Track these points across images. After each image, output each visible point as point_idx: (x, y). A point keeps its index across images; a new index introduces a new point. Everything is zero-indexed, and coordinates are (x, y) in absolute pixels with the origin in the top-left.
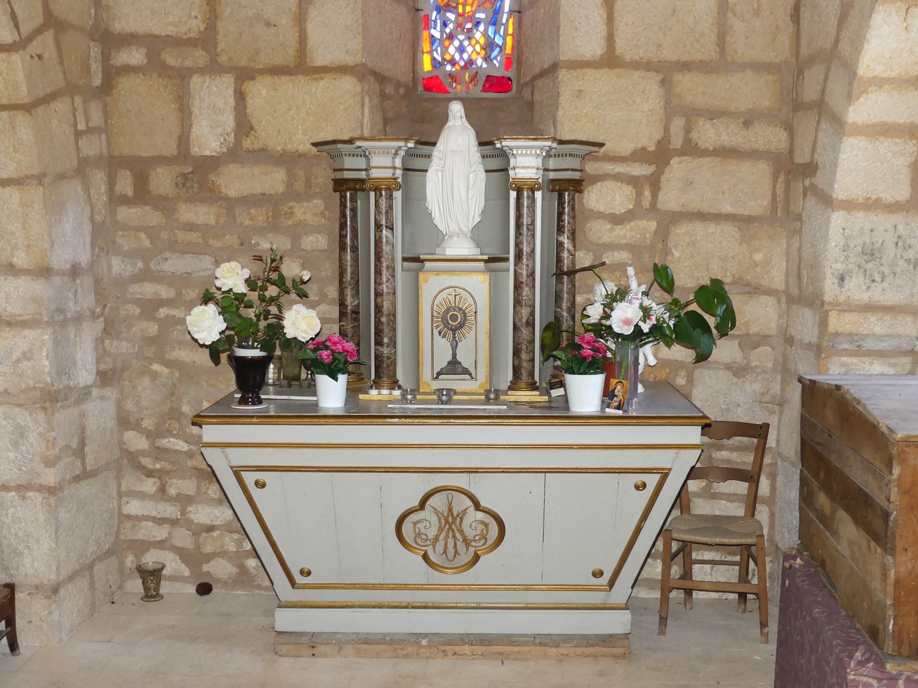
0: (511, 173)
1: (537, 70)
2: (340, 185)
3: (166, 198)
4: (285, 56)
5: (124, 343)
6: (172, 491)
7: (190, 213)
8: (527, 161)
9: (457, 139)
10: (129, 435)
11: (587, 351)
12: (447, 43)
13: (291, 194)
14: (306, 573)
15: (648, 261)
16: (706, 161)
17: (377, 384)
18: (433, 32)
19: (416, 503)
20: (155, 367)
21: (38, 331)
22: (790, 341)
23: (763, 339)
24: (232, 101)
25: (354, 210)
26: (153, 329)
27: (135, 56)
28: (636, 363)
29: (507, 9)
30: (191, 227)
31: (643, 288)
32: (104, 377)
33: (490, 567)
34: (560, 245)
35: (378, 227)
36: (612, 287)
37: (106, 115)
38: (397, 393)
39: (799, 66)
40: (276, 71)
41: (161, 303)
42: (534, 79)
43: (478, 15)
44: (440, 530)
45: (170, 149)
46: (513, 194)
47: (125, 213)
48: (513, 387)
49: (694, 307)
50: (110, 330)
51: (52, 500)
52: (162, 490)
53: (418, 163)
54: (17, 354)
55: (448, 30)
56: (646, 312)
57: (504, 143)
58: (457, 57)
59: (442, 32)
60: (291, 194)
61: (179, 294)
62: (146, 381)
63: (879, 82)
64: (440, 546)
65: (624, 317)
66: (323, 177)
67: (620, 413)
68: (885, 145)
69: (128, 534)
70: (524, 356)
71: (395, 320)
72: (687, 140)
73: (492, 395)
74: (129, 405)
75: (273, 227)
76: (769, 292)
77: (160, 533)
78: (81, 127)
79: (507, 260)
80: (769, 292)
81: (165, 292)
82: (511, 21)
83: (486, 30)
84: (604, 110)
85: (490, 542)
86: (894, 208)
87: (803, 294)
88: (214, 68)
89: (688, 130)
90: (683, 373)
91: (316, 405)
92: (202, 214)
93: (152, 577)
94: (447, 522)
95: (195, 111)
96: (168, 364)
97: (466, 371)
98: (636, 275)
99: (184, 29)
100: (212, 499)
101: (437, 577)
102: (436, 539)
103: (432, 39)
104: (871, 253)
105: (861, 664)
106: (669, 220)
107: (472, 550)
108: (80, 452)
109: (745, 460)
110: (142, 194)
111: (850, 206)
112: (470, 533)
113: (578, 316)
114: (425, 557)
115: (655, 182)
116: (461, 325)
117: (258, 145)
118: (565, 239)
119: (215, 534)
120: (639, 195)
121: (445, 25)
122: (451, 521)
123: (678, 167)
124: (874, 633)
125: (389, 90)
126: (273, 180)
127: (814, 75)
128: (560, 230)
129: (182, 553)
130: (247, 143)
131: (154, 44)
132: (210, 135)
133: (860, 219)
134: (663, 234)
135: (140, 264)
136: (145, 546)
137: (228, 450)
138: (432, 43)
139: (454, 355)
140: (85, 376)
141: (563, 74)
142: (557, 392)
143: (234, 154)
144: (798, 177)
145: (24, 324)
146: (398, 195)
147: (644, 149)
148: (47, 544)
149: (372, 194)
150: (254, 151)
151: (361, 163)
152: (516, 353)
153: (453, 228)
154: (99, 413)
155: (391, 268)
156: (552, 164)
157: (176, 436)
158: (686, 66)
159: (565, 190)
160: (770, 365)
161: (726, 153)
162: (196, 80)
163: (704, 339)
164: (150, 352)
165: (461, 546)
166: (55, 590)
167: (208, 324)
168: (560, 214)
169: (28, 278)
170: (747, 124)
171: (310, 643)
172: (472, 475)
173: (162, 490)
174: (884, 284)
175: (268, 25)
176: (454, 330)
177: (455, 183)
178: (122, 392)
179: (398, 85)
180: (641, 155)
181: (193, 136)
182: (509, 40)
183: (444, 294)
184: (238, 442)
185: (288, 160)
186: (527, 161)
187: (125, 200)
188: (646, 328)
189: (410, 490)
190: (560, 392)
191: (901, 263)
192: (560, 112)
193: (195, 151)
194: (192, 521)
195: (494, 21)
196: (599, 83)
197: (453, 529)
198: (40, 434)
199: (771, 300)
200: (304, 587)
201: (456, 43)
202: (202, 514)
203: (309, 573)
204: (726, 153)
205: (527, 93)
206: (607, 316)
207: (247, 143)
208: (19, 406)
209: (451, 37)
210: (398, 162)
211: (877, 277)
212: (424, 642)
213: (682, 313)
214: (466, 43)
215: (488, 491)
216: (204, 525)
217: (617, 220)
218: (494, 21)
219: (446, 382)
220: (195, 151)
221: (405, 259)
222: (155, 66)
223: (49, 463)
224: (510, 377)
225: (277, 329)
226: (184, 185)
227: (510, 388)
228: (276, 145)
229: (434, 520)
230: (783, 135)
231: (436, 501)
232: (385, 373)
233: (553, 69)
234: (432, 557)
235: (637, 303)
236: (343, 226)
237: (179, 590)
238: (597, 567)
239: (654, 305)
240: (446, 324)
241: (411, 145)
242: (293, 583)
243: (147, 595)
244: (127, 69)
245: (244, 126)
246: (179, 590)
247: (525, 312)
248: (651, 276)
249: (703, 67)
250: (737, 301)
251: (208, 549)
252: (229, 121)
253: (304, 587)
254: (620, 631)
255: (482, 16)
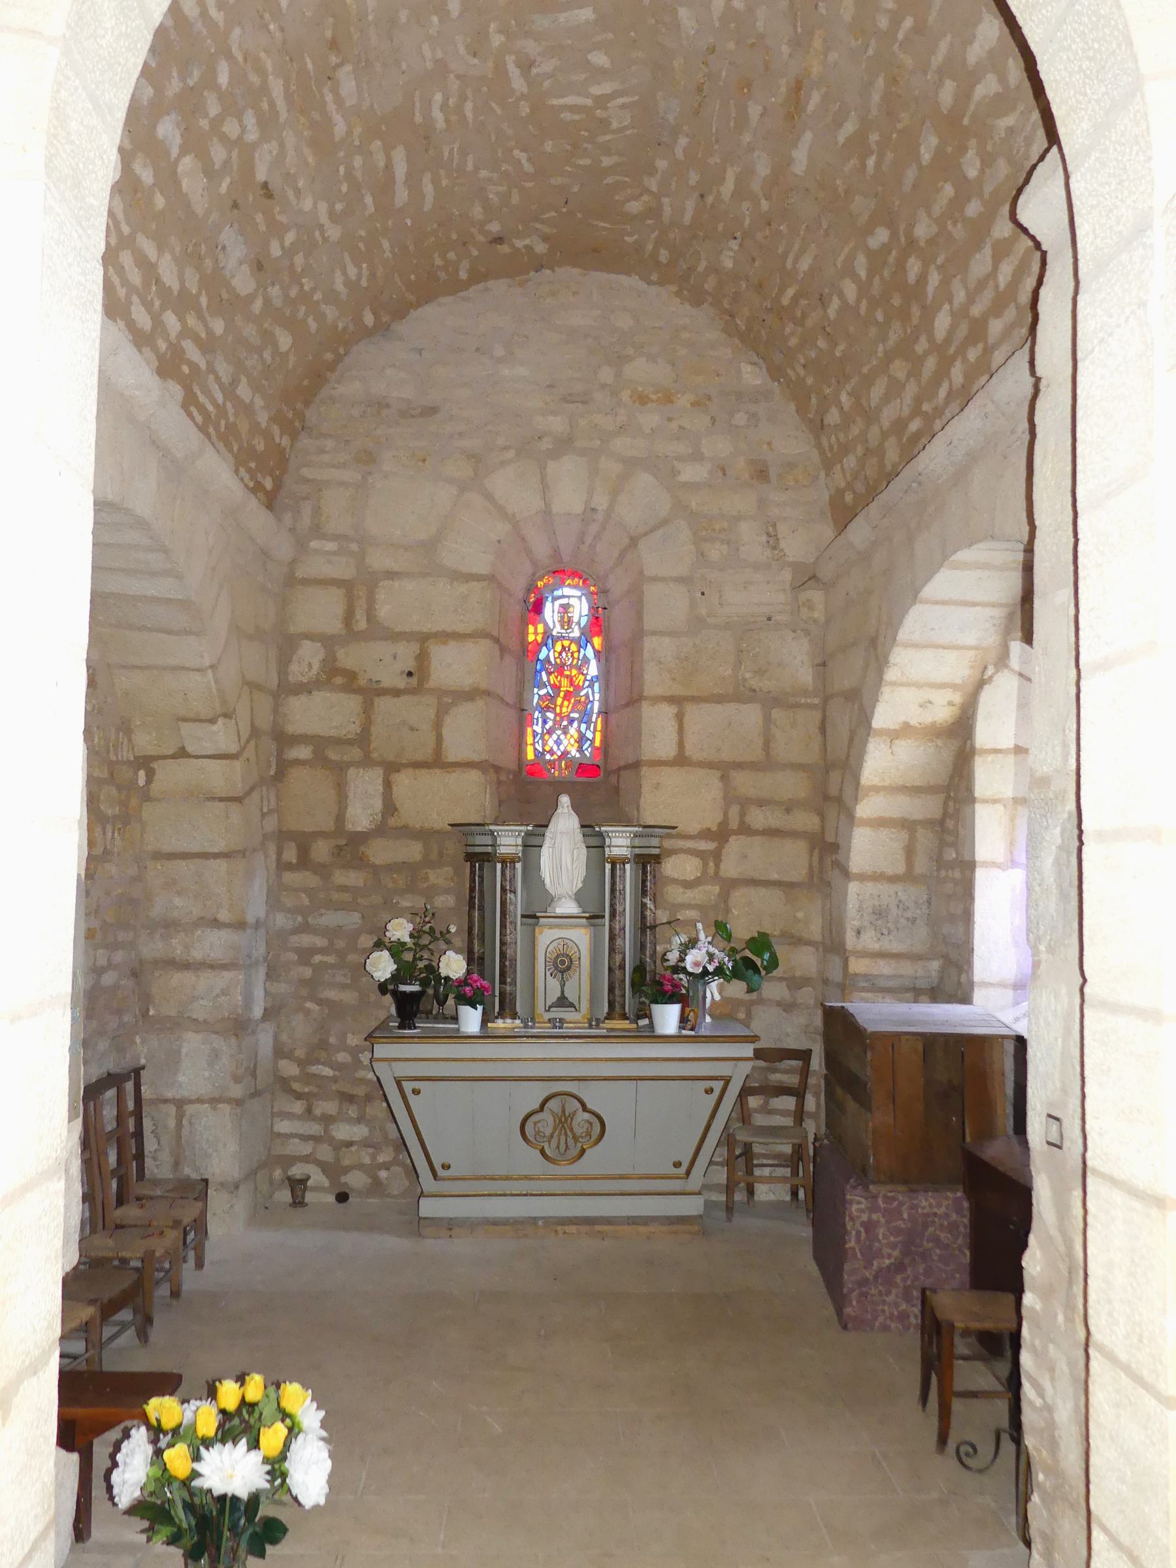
0: (607, 850)
1: (622, 763)
2: (471, 857)
3: (323, 866)
4: (425, 752)
5: (283, 985)
6: (318, 1112)
7: (341, 877)
8: (620, 842)
9: (565, 823)
10: (283, 1063)
11: (668, 987)
12: (546, 737)
13: (427, 862)
14: (446, 1167)
15: (712, 917)
16: (757, 840)
17: (501, 1015)
18: (535, 727)
19: (537, 1106)
20: (308, 1005)
21: (234, 972)
22: (826, 982)
23: (805, 981)
24: (381, 788)
25: (481, 877)
26: (307, 972)
27: (303, 752)
28: (704, 997)
29: (596, 710)
30: (343, 889)
31: (710, 939)
32: (268, 1014)
33: (595, 1160)
34: (644, 905)
35: (503, 890)
36: (684, 938)
37: (278, 798)
38: (518, 1022)
39: (828, 766)
40: (417, 765)
41: (314, 951)
42: (620, 769)
43: (572, 715)
44: (555, 1129)
45: (328, 824)
46: (608, 866)
47: (289, 877)
48: (609, 1017)
49: (748, 953)
50: (272, 974)
51: (238, 1111)
52: (309, 1110)
53: (535, 841)
54: (218, 991)
55: (547, 727)
56: (711, 957)
57: (603, 829)
58: (555, 748)
59: (543, 727)
60: (427, 862)
61: (331, 943)
62: (300, 1017)
63: (876, 789)
64: (554, 1142)
65: (694, 959)
66: (454, 849)
67: (693, 1033)
68: (884, 834)
69: (278, 1150)
70: (617, 992)
71: (1027, 846)
72: (742, 822)
73: (594, 1022)
74: (284, 1037)
75: (411, 889)
76: (809, 943)
77: (306, 1149)
78: (265, 810)
79: (603, 917)
80: (809, 943)
81: (320, 942)
82: (599, 720)
83: (579, 727)
84: (677, 800)
85: (594, 1137)
86: (893, 879)
87: (833, 945)
88: (367, 762)
89: (743, 814)
90: (743, 1009)
91: (458, 1030)
92: (353, 878)
93: (298, 1186)
94: (560, 1121)
95: (351, 795)
96: (320, 1002)
97: (572, 1005)
98: (704, 929)
99: (344, 732)
100: (351, 1118)
101: (552, 1169)
102: (552, 1136)
103: (535, 734)
104: (879, 913)
105: (855, 1187)
106: (729, 885)
107: (579, 1145)
108: (254, 1075)
109: (793, 1080)
110: (304, 862)
111: (862, 878)
112: (578, 1131)
113: (658, 962)
114: (543, 1152)
115: (717, 856)
116: (569, 968)
117: (400, 823)
118: (647, 901)
119: (353, 1149)
120: (705, 865)
121: (545, 722)
122: (564, 1121)
123: (735, 845)
124: (864, 1171)
125: (503, 777)
126: (413, 851)
127: (835, 776)
128: (644, 893)
129: (324, 1167)
130: (392, 822)
131: (320, 743)
132: (361, 816)
133: (870, 888)
134: (725, 896)
135: (300, 919)
136: (293, 1160)
137: (393, 1064)
138: (534, 737)
139: (563, 992)
140: (258, 1012)
141: (644, 770)
142: (644, 1022)
143: (381, 830)
144: (827, 852)
145: (224, 967)
146: (519, 866)
147: (709, 829)
148: (233, 1147)
149: (499, 866)
150: (397, 828)
151: (488, 840)
152: (611, 990)
153: (560, 891)
154: (265, 1040)
155: (514, 923)
156: (637, 842)
157: (324, 1064)
158: (739, 766)
159: (646, 862)
160: (812, 1002)
161: (772, 833)
162: (352, 772)
163: (756, 977)
164: (304, 992)
165: (571, 1142)
166: (237, 1187)
167: (383, 966)
168: (644, 881)
169: (230, 930)
170: (788, 811)
171: (450, 1226)
172: (581, 1083)
173: (309, 1110)
174: (891, 937)
175: (412, 729)
176: (562, 972)
177: (563, 858)
178: (278, 1026)
179: (509, 772)
180: (706, 834)
181: (348, 815)
182: (598, 735)
183: (555, 944)
184: (404, 1056)
185: (424, 835)
186: (620, 842)
187: (289, 867)
188: (711, 968)
189: (532, 1096)
190: (646, 1022)
191: (902, 920)
192: (642, 799)
193: (349, 827)
194: (334, 1138)
195: (585, 718)
196: (672, 778)
197: (563, 1127)
198: (232, 1056)
199: (812, 949)
200: (444, 1179)
201: (555, 737)
202: (343, 1132)
203: (449, 1167)
204: (772, 833)
205: (613, 779)
206: (682, 960)
207: (392, 822)
208: (216, 1033)
209: (550, 732)
210: (519, 841)
211: (885, 931)
212: (540, 1223)
213: (738, 957)
214: (562, 737)
215: (594, 1096)
216: (342, 1141)
217: (688, 885)
218: (585, 718)
219: (557, 1013)
220: (349, 827)
221: (523, 916)
222: (320, 760)
223: (237, 1080)
224: (606, 1009)
225: (432, 970)
226: (339, 854)
227: (606, 1018)
228: (416, 823)
229: (551, 1120)
230: (816, 820)
231: (553, 1104)
232: (507, 1008)
233: (636, 765)
234: (548, 1152)
235: (704, 951)
236: (472, 889)
237: (320, 1197)
238: (677, 1159)
239: (716, 951)
240: (556, 968)
241: (530, 828)
242: (435, 1175)
243: (294, 1202)
244: (297, 762)
245: (390, 807)
246: (320, 1197)
247: (618, 958)
248: (713, 929)
249: (753, 766)
250: (781, 951)
251: (346, 1162)
252: (378, 804)
253: (444, 1179)
254: (694, 1213)
255: (576, 715)
